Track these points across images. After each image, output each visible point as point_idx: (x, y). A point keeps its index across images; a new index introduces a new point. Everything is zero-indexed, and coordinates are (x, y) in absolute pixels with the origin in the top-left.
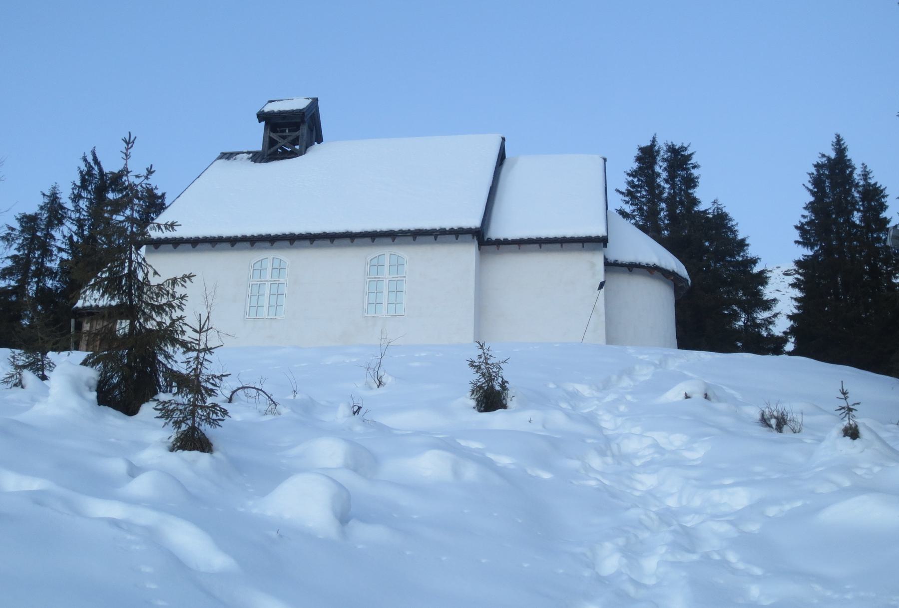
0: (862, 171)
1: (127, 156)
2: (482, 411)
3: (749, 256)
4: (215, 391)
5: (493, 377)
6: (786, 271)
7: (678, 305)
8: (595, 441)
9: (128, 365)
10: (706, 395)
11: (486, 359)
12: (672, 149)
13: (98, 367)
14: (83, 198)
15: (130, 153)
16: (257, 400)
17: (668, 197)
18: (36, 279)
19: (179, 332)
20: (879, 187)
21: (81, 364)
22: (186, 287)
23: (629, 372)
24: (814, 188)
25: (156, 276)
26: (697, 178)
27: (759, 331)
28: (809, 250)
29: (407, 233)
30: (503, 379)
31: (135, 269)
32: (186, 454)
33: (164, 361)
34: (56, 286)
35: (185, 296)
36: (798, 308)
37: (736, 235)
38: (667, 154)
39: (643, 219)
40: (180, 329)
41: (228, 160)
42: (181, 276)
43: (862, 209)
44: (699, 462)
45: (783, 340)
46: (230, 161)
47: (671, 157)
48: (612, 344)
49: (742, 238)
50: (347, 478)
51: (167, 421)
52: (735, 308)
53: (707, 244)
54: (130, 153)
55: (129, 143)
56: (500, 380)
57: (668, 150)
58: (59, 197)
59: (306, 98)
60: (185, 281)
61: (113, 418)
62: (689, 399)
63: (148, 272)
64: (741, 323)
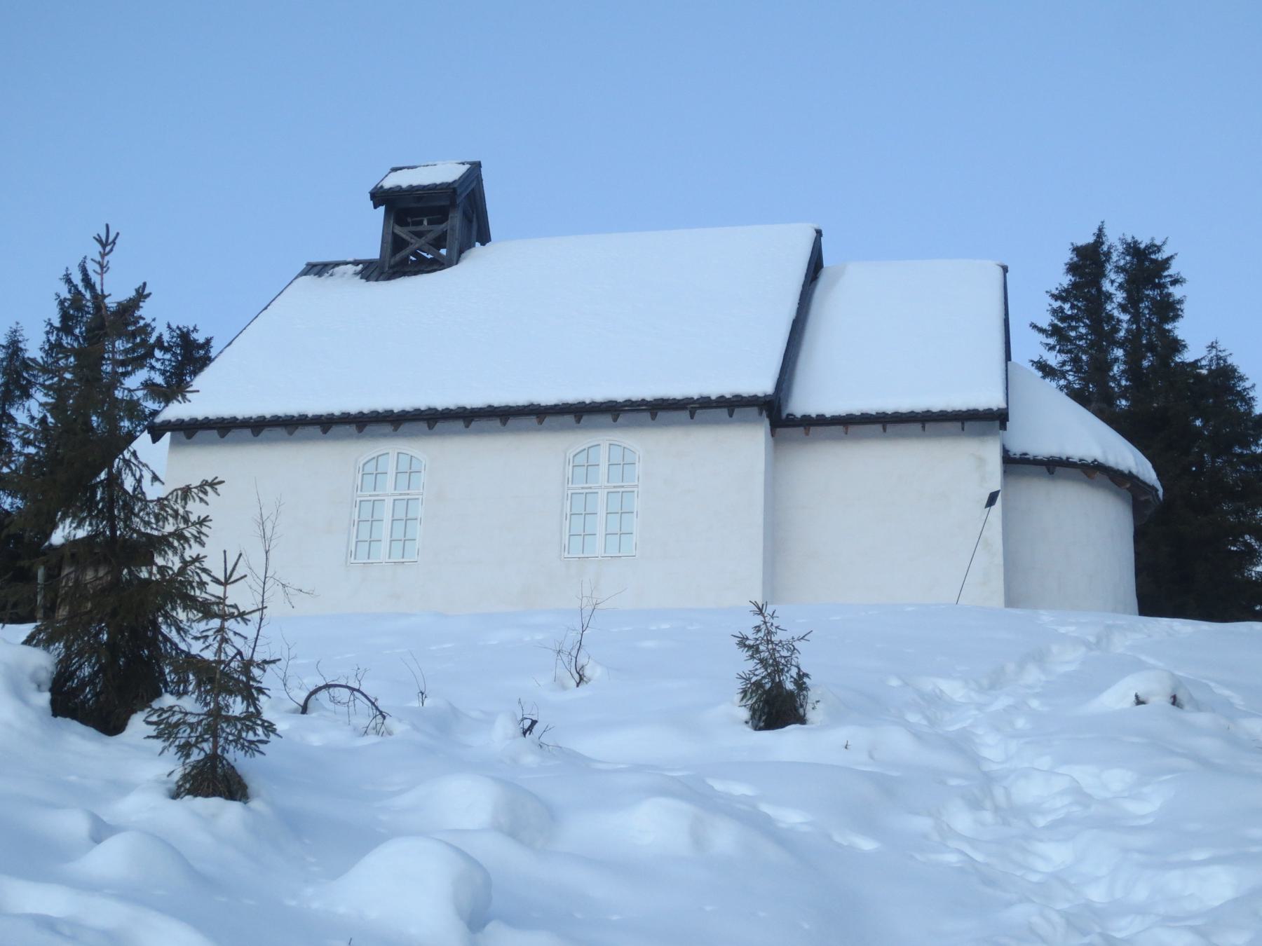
2: (761, 729)
4: (266, 691)
5: (781, 667)
7: (1140, 536)
11: (769, 633)
12: (1134, 250)
15: (108, 262)
19: (195, 584)
23: (1040, 658)
25: (157, 484)
26: (1180, 302)
29: (639, 405)
30: (799, 669)
33: (174, 635)
35: (205, 519)
37: (1252, 407)
38: (1124, 259)
39: (1080, 379)
40: (197, 579)
41: (320, 276)
42: (198, 483)
44: (1150, 821)
46: (323, 278)
47: (1132, 264)
48: (1017, 607)
54: (108, 262)
56: (794, 672)
57: (1127, 250)
58: (23, 347)
59: (460, 162)
60: (205, 493)
62: (1143, 705)
63: (141, 476)
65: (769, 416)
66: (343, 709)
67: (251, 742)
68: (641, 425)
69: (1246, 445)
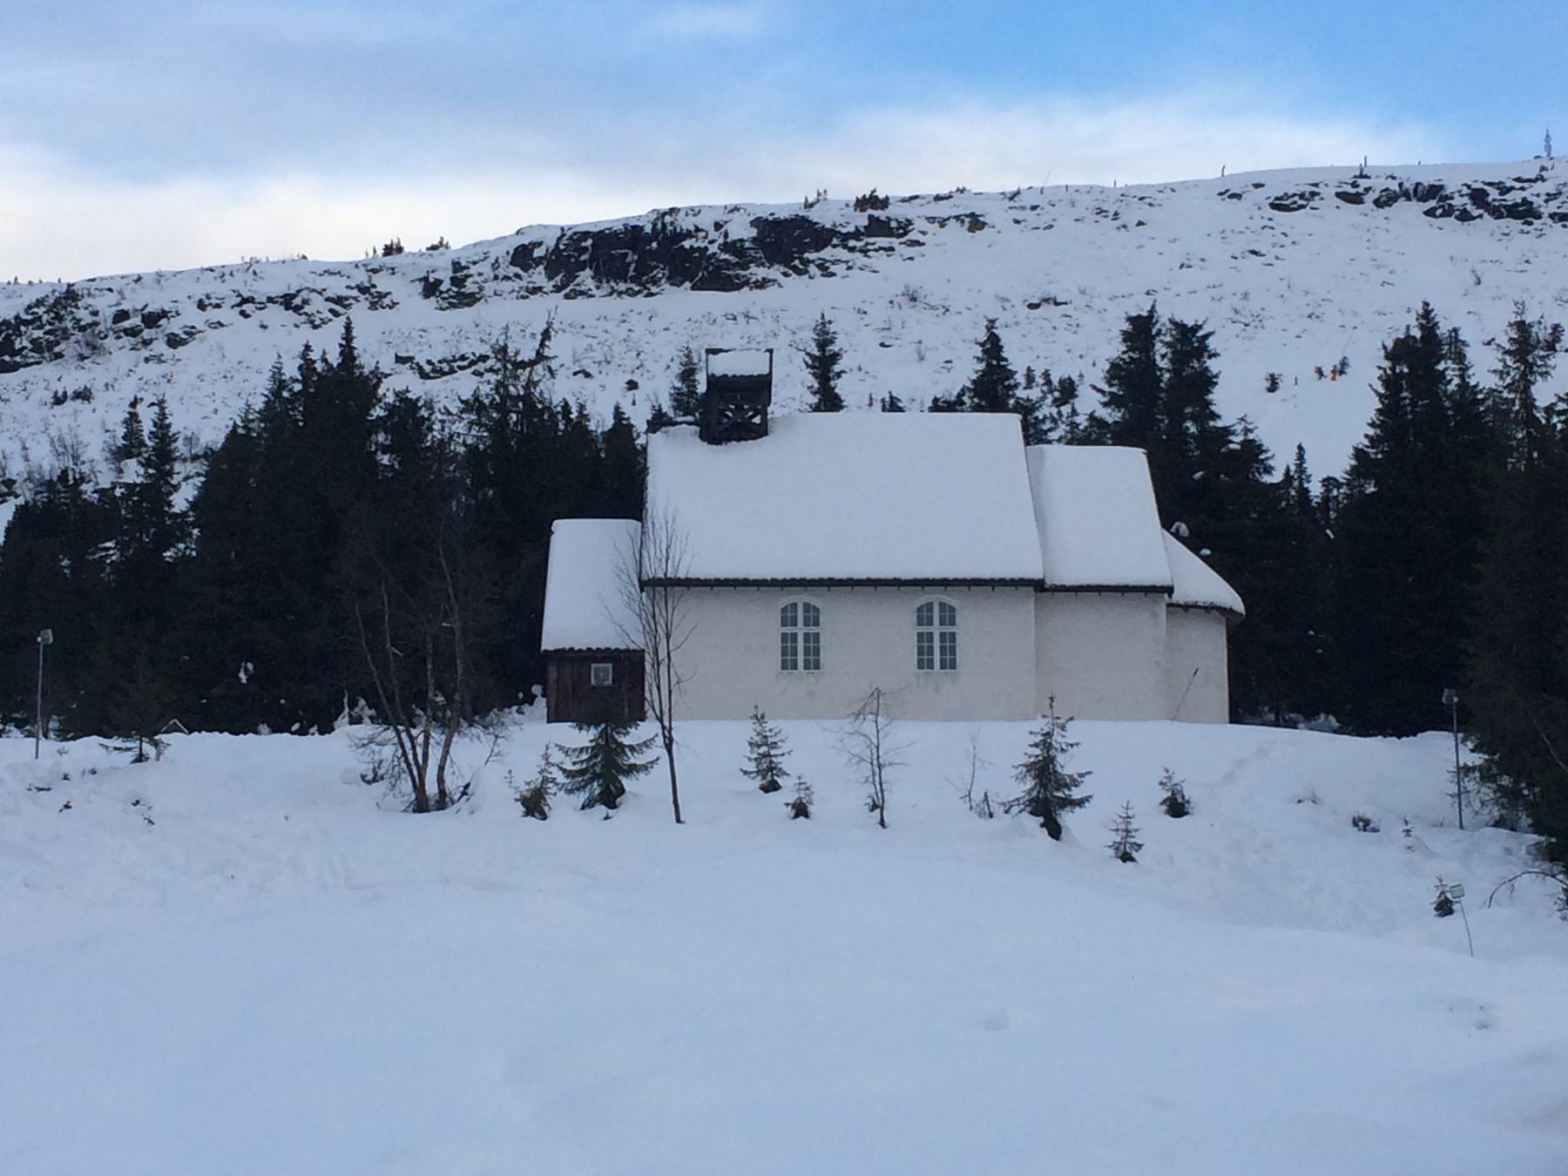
6: (1277, 199)
12: (1179, 326)
26: (1216, 376)
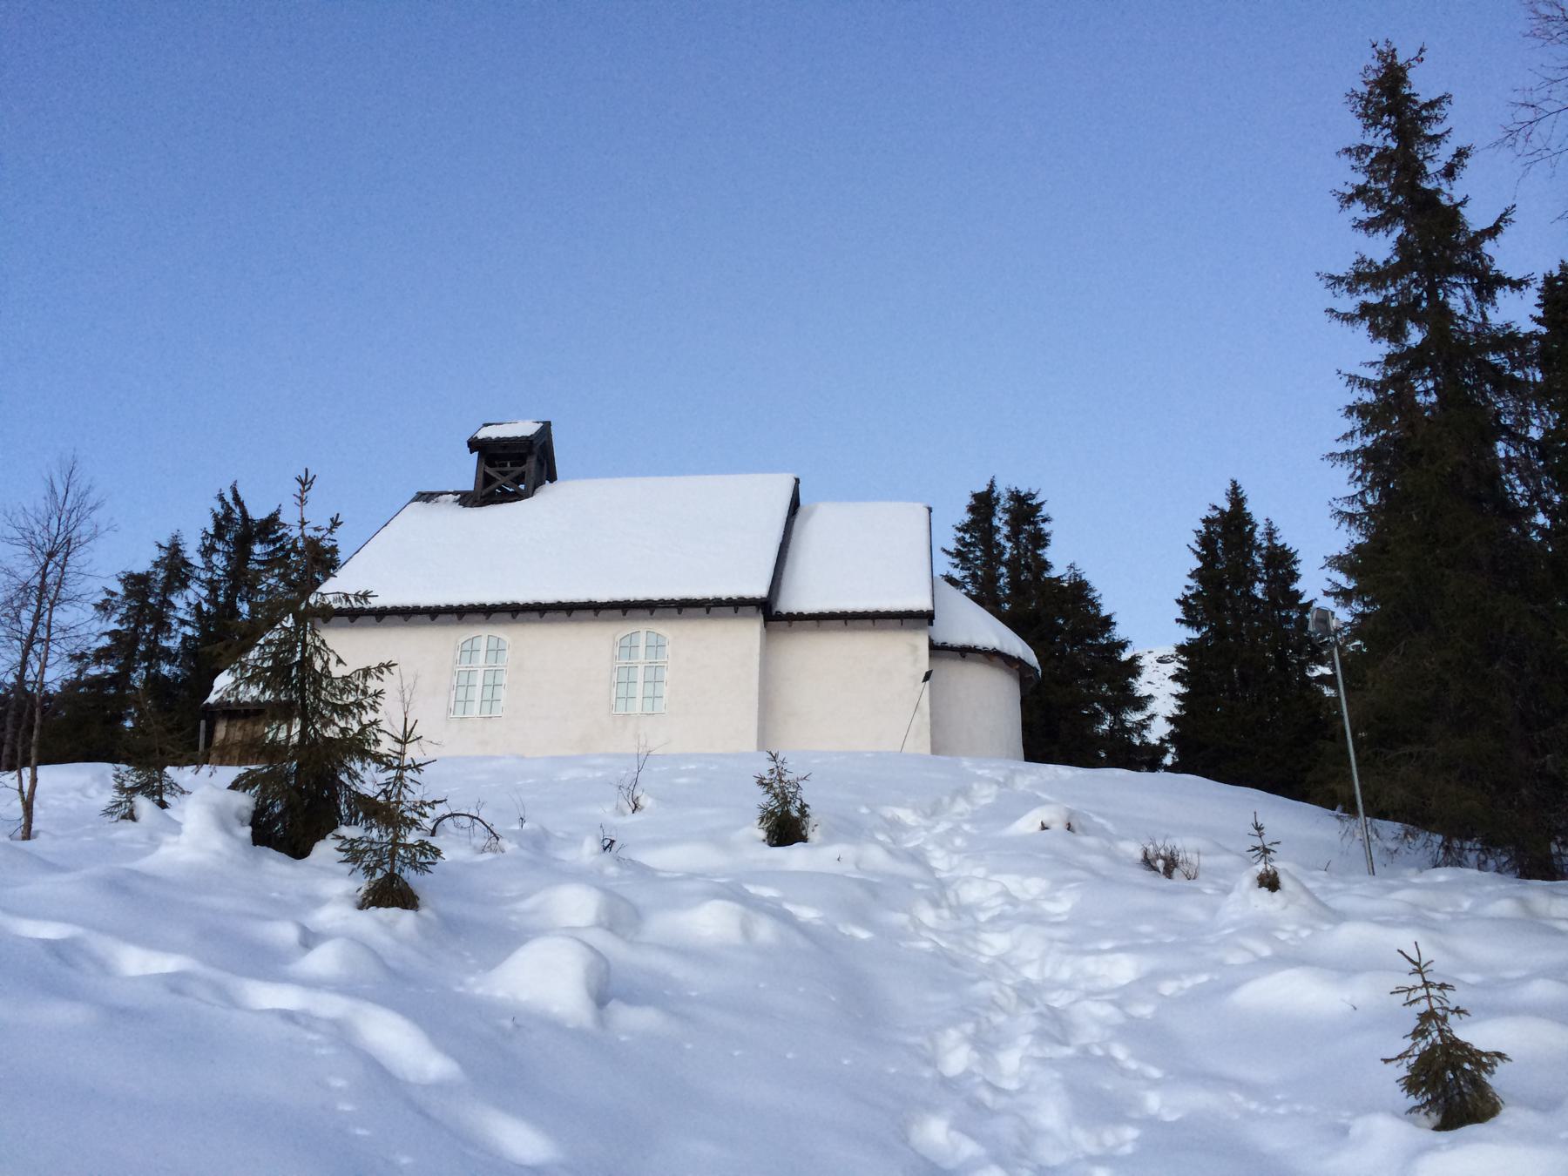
0: (1266, 529)
1: (303, 501)
2: (774, 846)
3: (1116, 638)
5: (789, 799)
7: (1025, 703)
8: (926, 887)
9: (297, 788)
10: (1069, 824)
11: (779, 774)
13: (253, 791)
14: (219, 551)
16: (471, 831)
17: (1009, 559)
18: (146, 664)
19: (371, 741)
20: (1289, 550)
21: (229, 788)
22: (382, 681)
23: (964, 792)
24: (1202, 550)
25: (341, 665)
27: (1129, 738)
28: (1195, 632)
30: (802, 801)
31: (311, 655)
32: (382, 912)
34: (175, 673)
35: (380, 692)
36: (1180, 708)
39: (977, 588)
40: (374, 737)
41: (428, 502)
43: (1266, 578)
44: (1065, 918)
45: (1160, 751)
49: (1108, 614)
50: (601, 940)
51: (356, 866)
52: (1097, 706)
53: (1061, 621)
55: (305, 483)
56: (798, 803)
60: (382, 673)
61: (275, 865)
63: (329, 659)
64: (1105, 727)
65: (763, 613)
66: (465, 832)
67: (424, 864)
68: (671, 618)
69: (1095, 637)
